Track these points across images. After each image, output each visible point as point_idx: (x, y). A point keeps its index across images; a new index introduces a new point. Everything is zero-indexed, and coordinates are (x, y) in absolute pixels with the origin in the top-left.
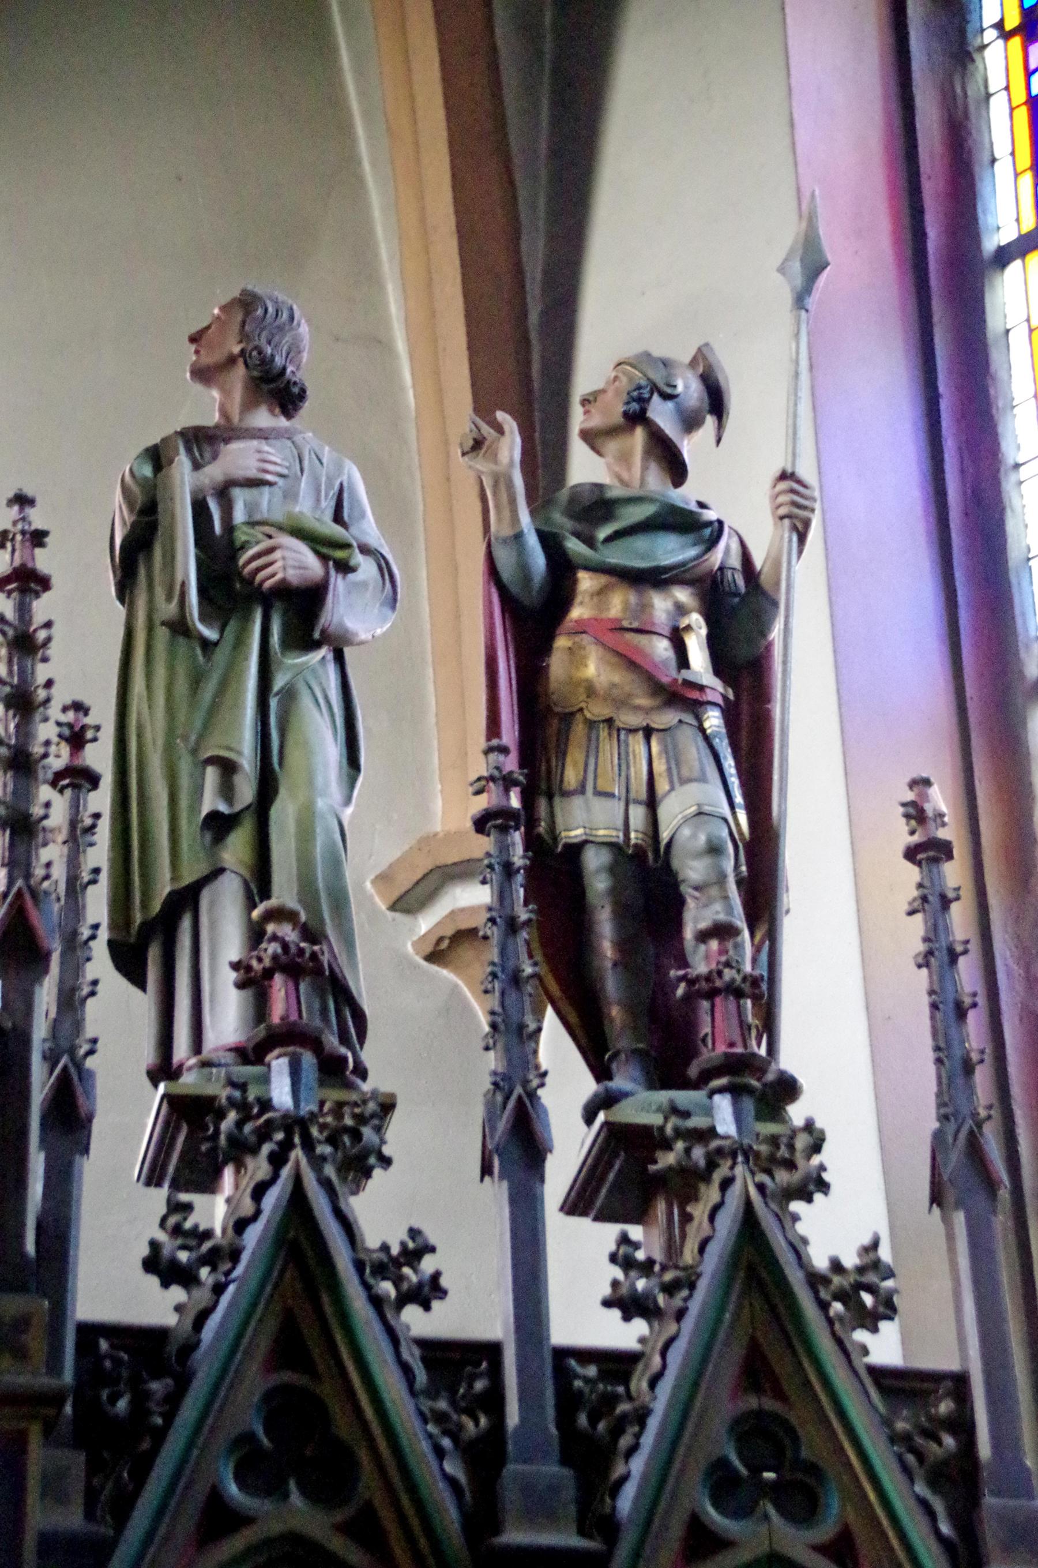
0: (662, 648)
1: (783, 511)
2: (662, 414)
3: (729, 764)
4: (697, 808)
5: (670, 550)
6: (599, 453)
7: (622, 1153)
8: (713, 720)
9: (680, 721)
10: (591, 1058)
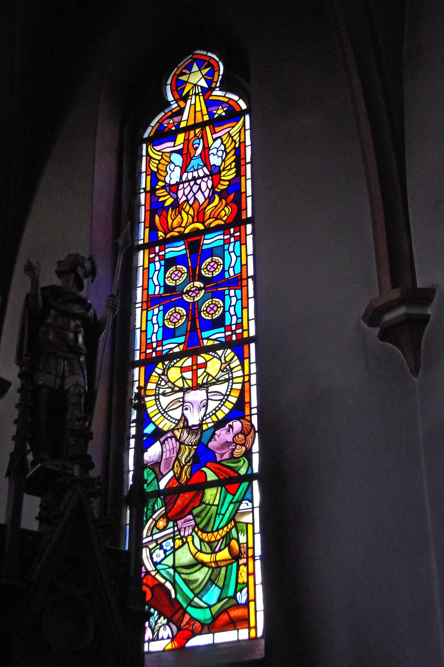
0: (71, 335)
1: (109, 305)
2: (80, 271)
3: (85, 371)
4: (77, 381)
5: (77, 309)
6: (60, 278)
7: (204, 469)
8: (82, 359)
9: (74, 357)
10: (126, 444)
